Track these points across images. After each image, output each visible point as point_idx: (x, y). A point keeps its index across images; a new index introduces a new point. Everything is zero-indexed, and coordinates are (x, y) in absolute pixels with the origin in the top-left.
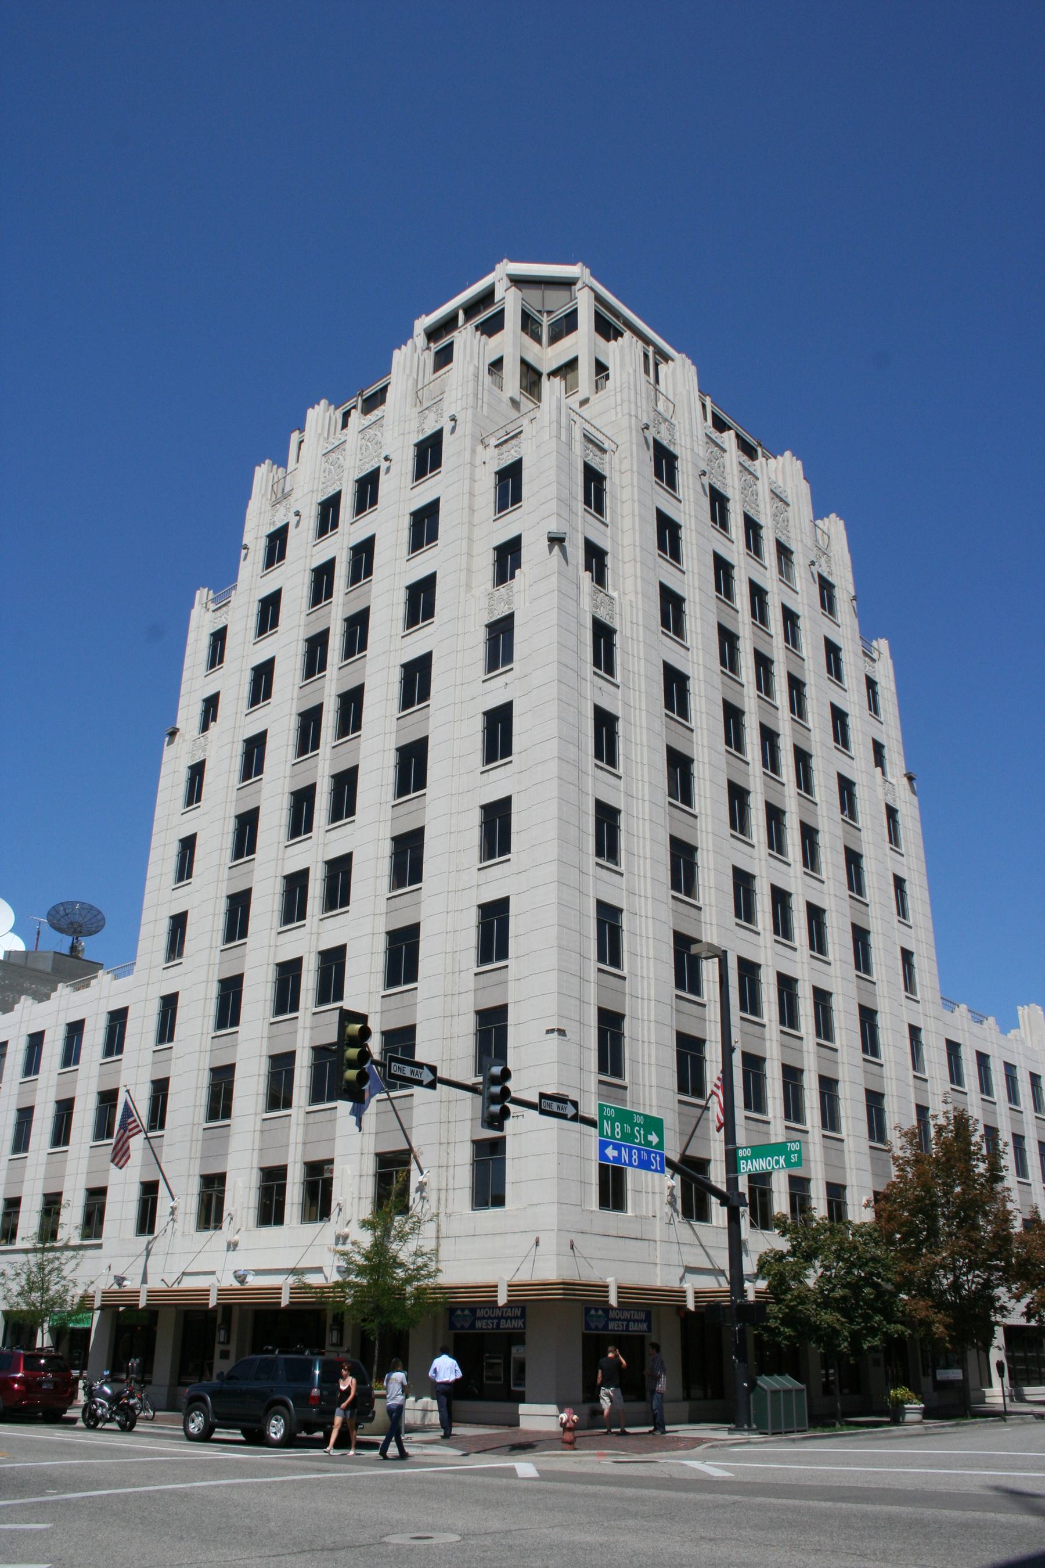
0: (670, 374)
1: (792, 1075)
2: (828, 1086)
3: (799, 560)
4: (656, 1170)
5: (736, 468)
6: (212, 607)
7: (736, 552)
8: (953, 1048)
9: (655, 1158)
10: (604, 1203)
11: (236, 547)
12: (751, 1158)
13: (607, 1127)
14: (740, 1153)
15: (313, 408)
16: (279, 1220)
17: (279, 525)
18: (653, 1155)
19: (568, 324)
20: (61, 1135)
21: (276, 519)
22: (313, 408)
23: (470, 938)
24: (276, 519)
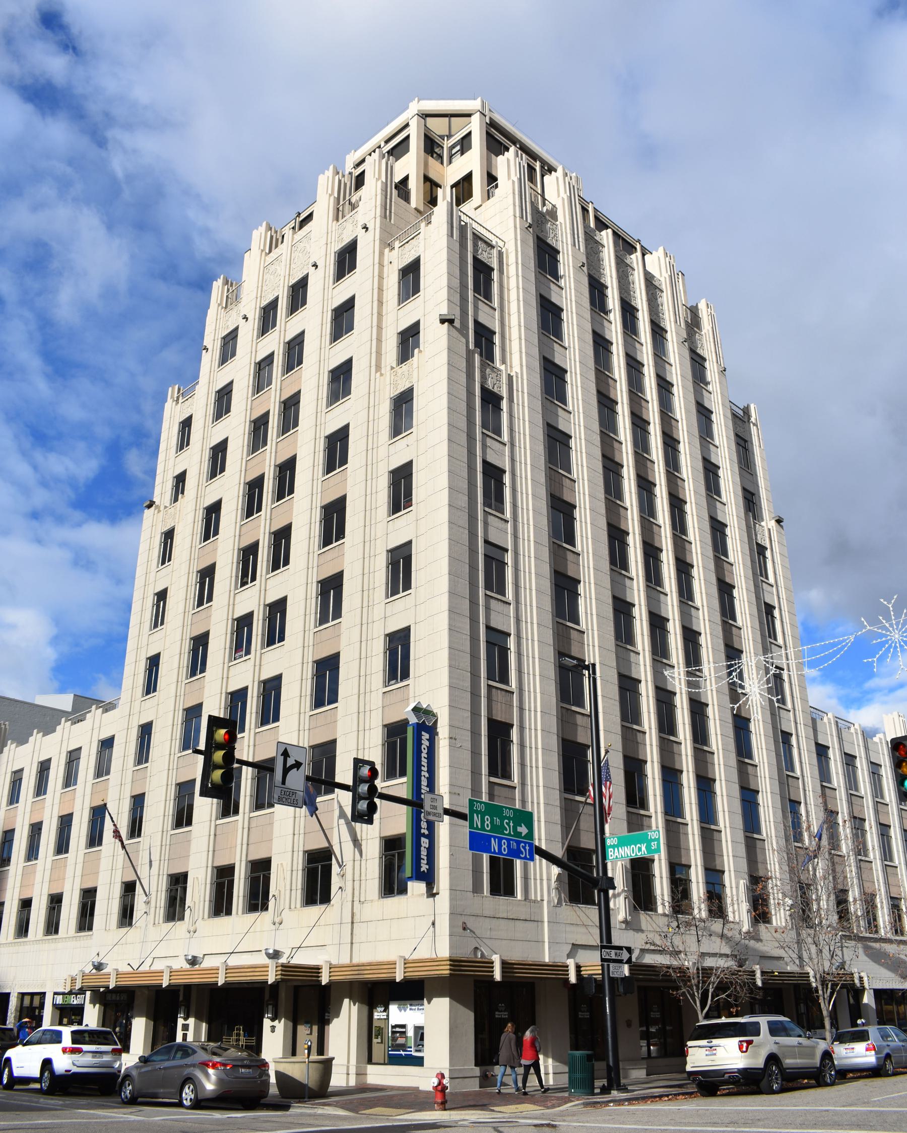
9: (524, 848)
13: (477, 820)
15: (257, 229)
18: (522, 844)
19: (465, 143)
20: (62, 846)
21: (229, 323)
22: (257, 229)
23: (378, 662)
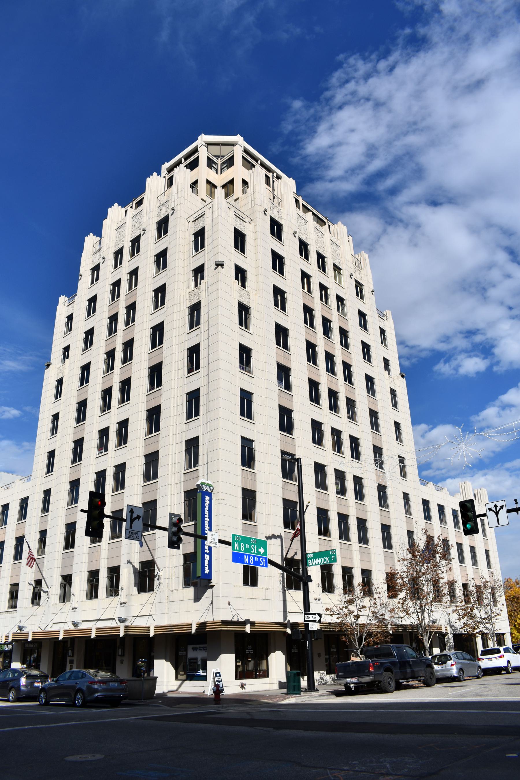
0: (279, 185)
1: (343, 518)
2: (362, 523)
3: (345, 273)
4: (263, 566)
5: (312, 230)
6: (67, 304)
7: (312, 268)
8: (426, 503)
9: (262, 560)
10: (246, 582)
11: (76, 276)
12: (313, 558)
14: (308, 556)
16: (96, 597)
17: (96, 264)
24: (94, 261)
